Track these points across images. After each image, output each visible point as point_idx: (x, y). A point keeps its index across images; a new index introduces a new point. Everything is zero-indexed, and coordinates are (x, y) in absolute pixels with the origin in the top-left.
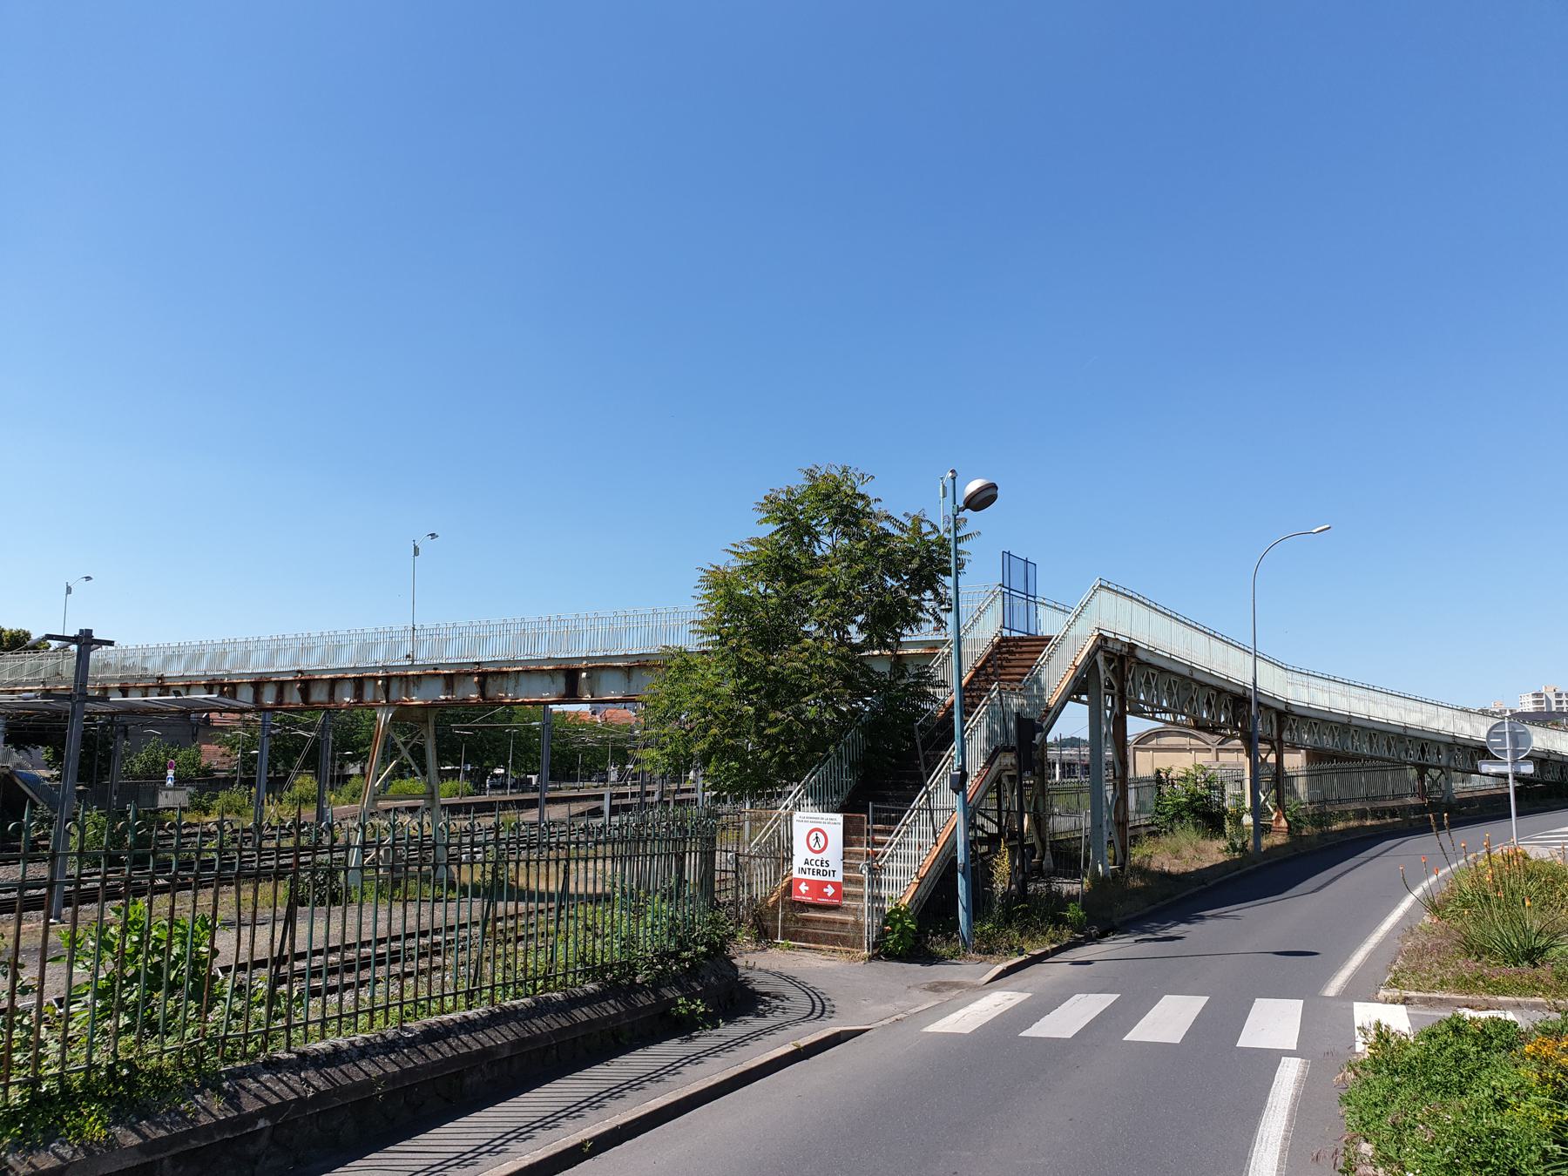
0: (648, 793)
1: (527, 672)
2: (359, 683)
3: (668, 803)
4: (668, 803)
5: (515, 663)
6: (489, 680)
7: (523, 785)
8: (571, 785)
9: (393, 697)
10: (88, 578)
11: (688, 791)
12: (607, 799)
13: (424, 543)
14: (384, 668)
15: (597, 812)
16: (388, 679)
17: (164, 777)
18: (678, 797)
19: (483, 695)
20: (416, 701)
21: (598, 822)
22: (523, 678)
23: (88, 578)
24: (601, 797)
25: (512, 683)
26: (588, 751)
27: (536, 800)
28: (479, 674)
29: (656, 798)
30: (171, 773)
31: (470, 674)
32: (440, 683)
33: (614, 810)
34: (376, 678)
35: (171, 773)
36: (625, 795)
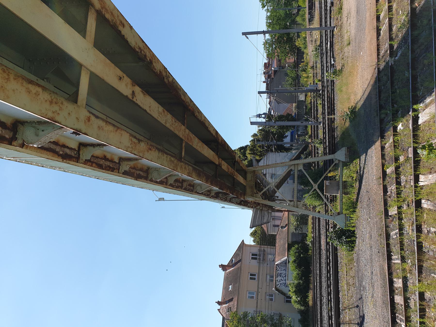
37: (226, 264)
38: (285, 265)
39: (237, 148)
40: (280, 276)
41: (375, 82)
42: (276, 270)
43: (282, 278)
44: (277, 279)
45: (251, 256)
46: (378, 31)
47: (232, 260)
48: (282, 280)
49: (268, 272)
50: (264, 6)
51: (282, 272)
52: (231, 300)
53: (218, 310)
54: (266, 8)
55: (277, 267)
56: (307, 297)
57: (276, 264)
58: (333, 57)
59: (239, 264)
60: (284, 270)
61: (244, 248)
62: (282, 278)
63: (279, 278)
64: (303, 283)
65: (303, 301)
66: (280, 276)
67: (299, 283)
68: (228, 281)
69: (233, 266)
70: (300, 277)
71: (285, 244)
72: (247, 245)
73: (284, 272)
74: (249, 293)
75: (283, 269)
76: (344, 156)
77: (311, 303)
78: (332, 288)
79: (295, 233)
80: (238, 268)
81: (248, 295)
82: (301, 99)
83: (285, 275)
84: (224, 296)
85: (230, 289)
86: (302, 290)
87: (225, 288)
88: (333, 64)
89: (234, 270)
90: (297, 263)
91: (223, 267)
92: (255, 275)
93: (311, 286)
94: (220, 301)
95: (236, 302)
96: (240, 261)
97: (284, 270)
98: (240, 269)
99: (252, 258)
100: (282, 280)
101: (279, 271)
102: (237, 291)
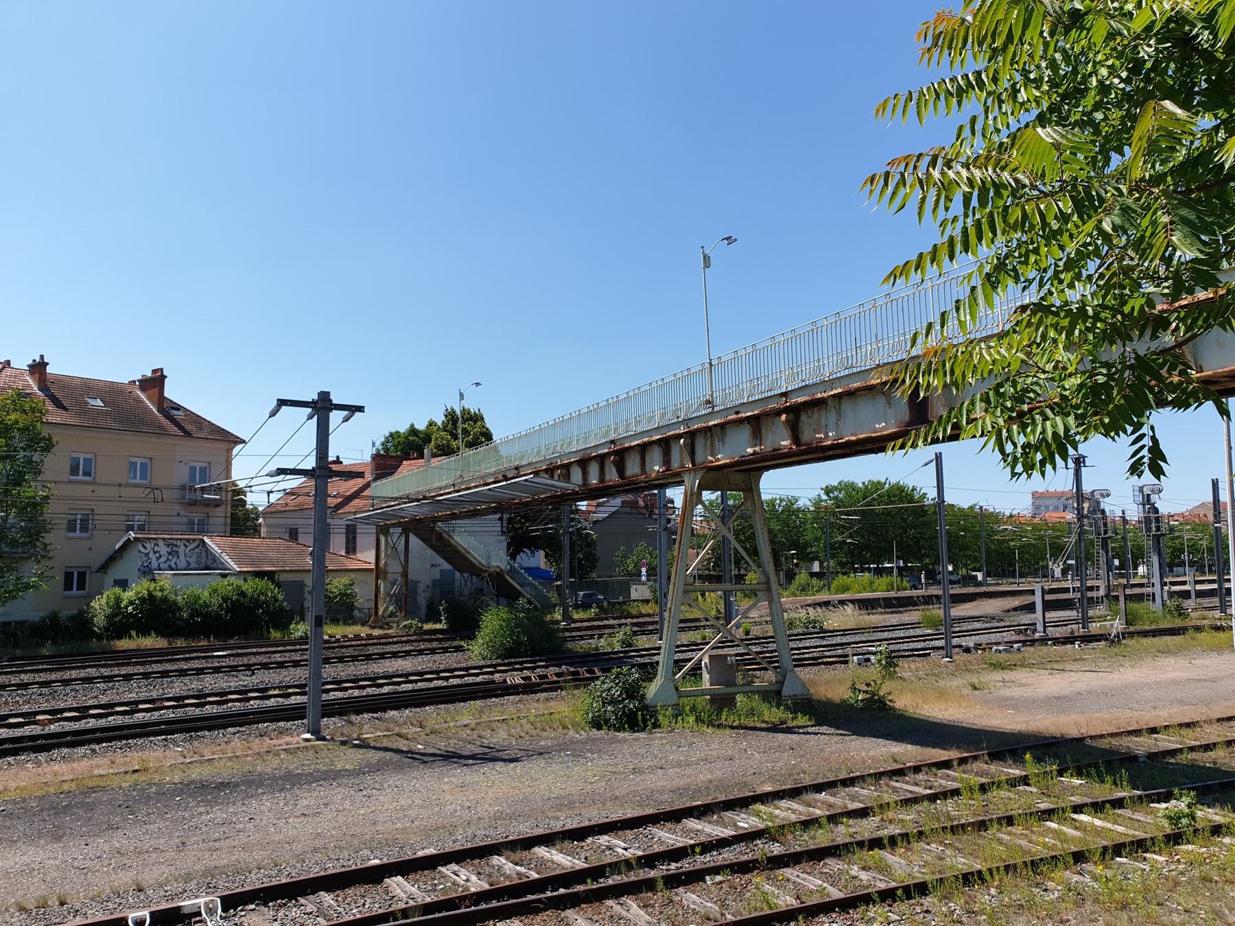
0: (1091, 589)
1: (850, 394)
2: (665, 444)
3: (1117, 598)
4: (1117, 598)
5: (832, 383)
6: (803, 417)
7: (969, 580)
8: (1011, 580)
9: (699, 459)
10: (478, 384)
11: (1142, 585)
12: (1038, 594)
13: (718, 251)
14: (686, 422)
15: (1031, 608)
16: (691, 435)
17: (640, 575)
18: (1128, 591)
19: (796, 439)
20: (722, 459)
21: (1026, 618)
22: (847, 404)
23: (478, 384)
24: (1032, 592)
25: (832, 417)
26: (1024, 549)
27: (937, 597)
28: (786, 410)
29: (1102, 592)
30: (644, 570)
31: (778, 413)
32: (745, 432)
33: (1048, 606)
34: (679, 436)
35: (644, 570)
36: (1067, 590)
37: (171, 392)
38: (202, 565)
39: (488, 426)
40: (169, 553)
41: (1045, 738)
42: (188, 540)
43: (163, 559)
44: (161, 543)
45: (198, 465)
46: (1137, 733)
47: (178, 407)
48: (158, 559)
49: (152, 519)
50: (828, 491)
51: (182, 557)
52: (58, 404)
53: (8, 362)
54: (824, 497)
55: (196, 544)
56: (144, 632)
57: (206, 540)
58: (266, 690)
59: (174, 429)
60: (189, 563)
61: (224, 446)
62: (163, 559)
63: (163, 549)
64: (182, 619)
65: (121, 624)
66: (169, 553)
67: (180, 609)
68: (112, 392)
69: (161, 409)
70: (196, 608)
71: (271, 563)
72: (230, 450)
73: (183, 564)
74: (143, 465)
75: (192, 560)
76: (792, 693)
77: (124, 644)
78: (369, 691)
79: (303, 590)
80: (163, 428)
81: (139, 461)
82: (633, 590)
83: (173, 566)
84: (65, 382)
85: (92, 402)
86: (156, 615)
87: (88, 387)
88: (868, 660)
89: (145, 411)
90: (238, 600)
91: (155, 382)
92: (143, 477)
93: (180, 643)
94: (49, 370)
95: (59, 420)
96: (187, 434)
97: (189, 563)
98: (162, 433)
99: (193, 469)
100: (158, 559)
101: (183, 547)
102: (92, 424)
